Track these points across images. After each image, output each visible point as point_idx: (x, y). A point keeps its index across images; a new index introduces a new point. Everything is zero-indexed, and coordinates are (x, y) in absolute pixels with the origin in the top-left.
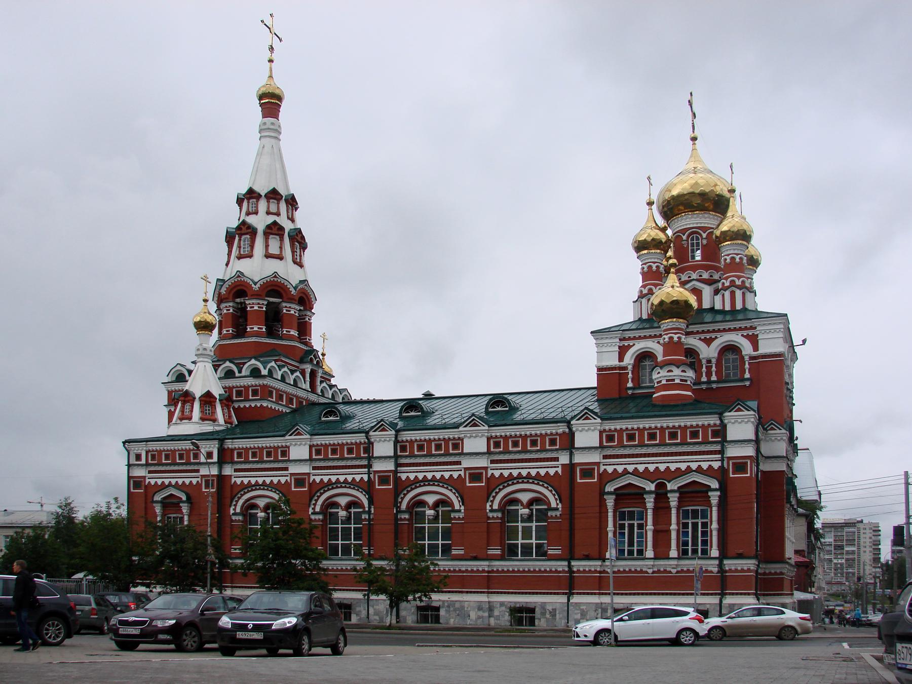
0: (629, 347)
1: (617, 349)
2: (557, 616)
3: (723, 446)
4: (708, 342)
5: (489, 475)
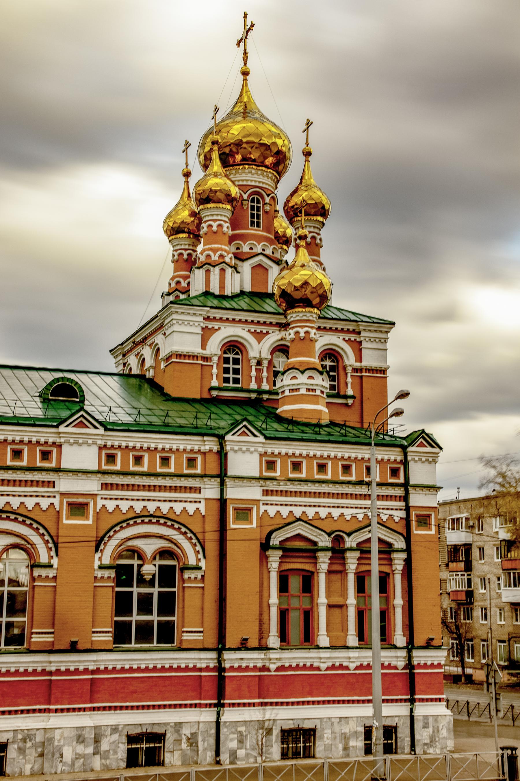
0: (214, 330)
1: (199, 331)
2: (200, 744)
3: (407, 492)
4: (260, 336)
5: (99, 507)
